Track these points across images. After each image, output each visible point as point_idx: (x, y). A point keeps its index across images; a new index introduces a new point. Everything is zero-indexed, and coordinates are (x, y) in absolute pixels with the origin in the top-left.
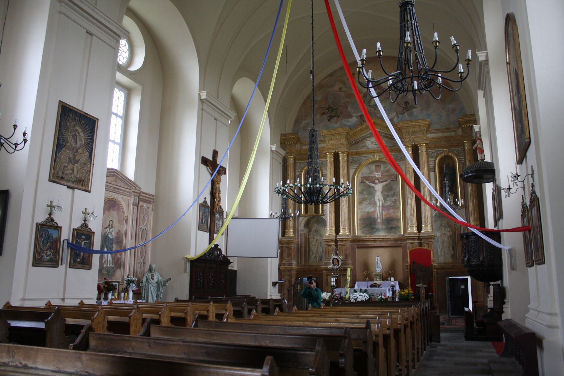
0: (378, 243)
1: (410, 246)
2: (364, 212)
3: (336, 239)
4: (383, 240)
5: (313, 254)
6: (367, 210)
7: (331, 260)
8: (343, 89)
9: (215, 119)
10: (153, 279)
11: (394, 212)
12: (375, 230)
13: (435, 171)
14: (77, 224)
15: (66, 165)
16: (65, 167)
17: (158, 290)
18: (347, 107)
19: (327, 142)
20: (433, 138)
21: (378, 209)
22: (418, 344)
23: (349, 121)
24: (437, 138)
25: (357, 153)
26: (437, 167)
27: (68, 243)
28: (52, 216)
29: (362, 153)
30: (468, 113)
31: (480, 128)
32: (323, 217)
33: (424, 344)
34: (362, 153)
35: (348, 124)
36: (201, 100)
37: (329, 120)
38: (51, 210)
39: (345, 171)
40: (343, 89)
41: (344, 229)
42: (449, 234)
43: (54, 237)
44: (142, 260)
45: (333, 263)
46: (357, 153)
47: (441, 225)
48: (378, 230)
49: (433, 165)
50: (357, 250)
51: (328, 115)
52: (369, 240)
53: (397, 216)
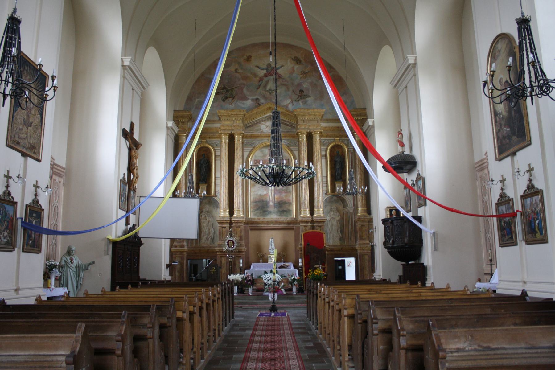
0: (271, 225)
1: (303, 229)
2: (257, 195)
3: (231, 221)
4: (277, 222)
5: (204, 235)
6: (259, 193)
7: (226, 242)
8: (240, 71)
9: (133, 89)
10: (72, 263)
11: (286, 196)
12: (267, 213)
13: (326, 159)
14: (29, 200)
15: (21, 127)
16: (20, 129)
17: (78, 275)
18: (242, 89)
19: (222, 122)
20: (326, 127)
21: (270, 192)
22: (219, 321)
23: (244, 104)
24: (329, 127)
25: (252, 136)
26: (328, 155)
27: (22, 221)
28: (9, 189)
29: (257, 136)
30: (357, 107)
31: (374, 122)
32: (215, 198)
33: (226, 320)
34: (257, 136)
35: (243, 106)
36: (123, 66)
37: (224, 101)
38: (8, 182)
39: (241, 153)
40: (240, 71)
41: (239, 210)
42: (338, 218)
43: (10, 215)
44: (54, 241)
45: (228, 244)
46: (252, 136)
47: (331, 210)
48: (270, 213)
49: (324, 153)
50: (250, 232)
51: (223, 95)
52: (263, 223)
53: (289, 200)
